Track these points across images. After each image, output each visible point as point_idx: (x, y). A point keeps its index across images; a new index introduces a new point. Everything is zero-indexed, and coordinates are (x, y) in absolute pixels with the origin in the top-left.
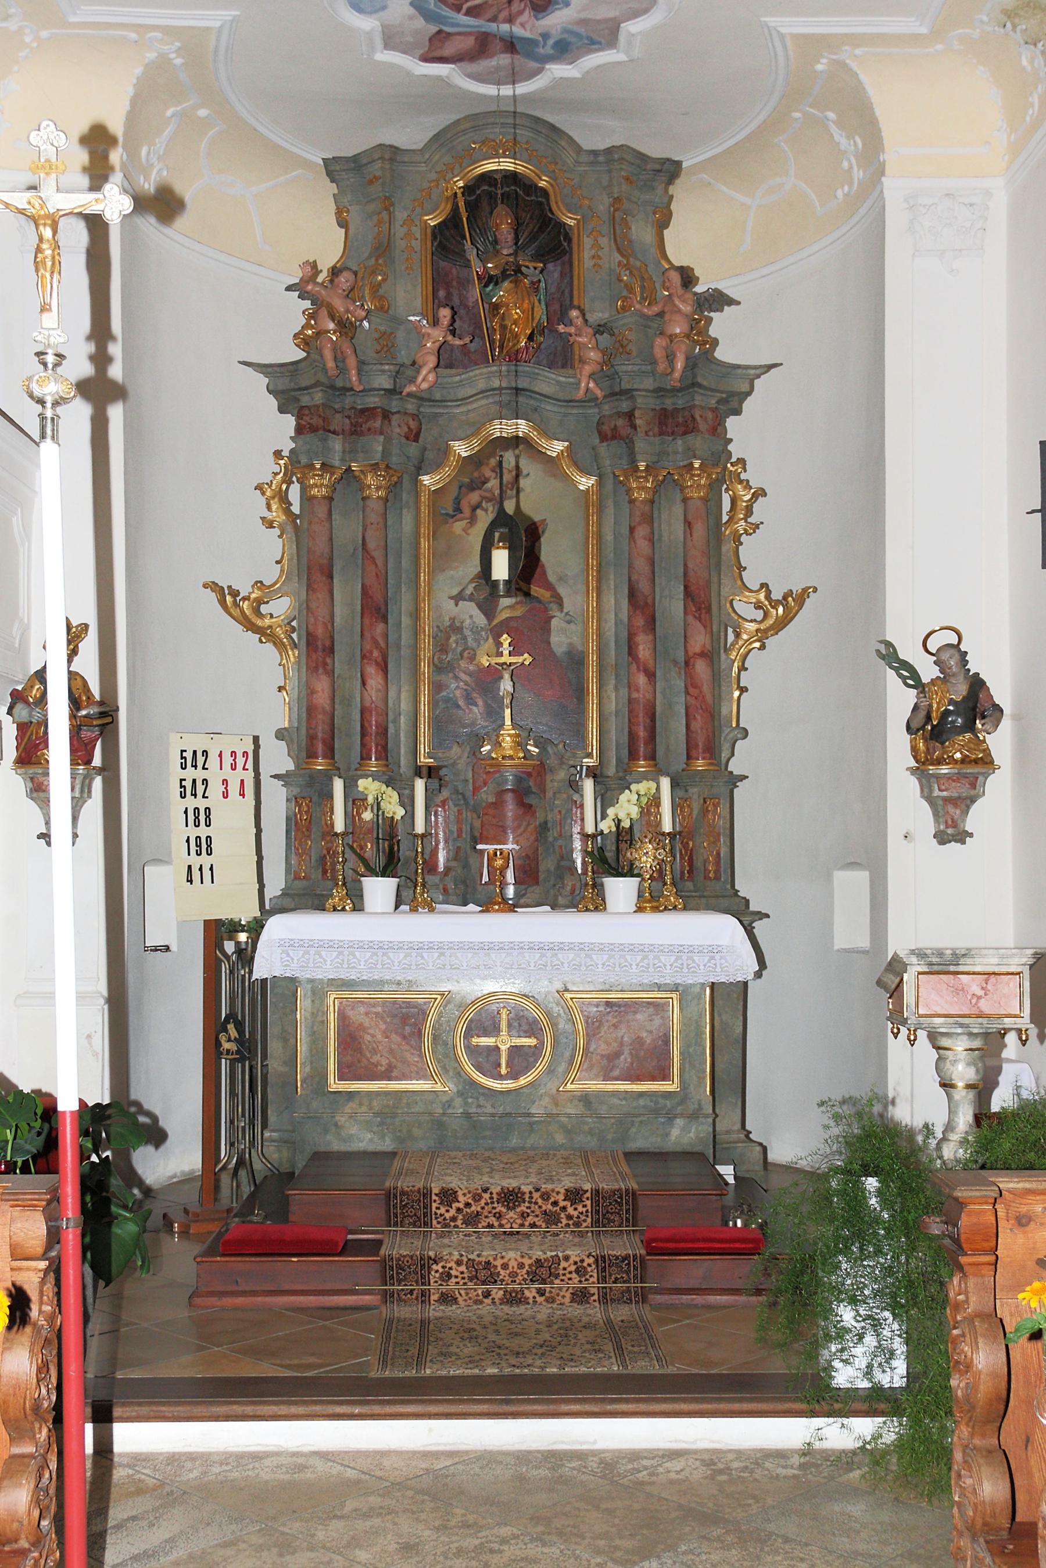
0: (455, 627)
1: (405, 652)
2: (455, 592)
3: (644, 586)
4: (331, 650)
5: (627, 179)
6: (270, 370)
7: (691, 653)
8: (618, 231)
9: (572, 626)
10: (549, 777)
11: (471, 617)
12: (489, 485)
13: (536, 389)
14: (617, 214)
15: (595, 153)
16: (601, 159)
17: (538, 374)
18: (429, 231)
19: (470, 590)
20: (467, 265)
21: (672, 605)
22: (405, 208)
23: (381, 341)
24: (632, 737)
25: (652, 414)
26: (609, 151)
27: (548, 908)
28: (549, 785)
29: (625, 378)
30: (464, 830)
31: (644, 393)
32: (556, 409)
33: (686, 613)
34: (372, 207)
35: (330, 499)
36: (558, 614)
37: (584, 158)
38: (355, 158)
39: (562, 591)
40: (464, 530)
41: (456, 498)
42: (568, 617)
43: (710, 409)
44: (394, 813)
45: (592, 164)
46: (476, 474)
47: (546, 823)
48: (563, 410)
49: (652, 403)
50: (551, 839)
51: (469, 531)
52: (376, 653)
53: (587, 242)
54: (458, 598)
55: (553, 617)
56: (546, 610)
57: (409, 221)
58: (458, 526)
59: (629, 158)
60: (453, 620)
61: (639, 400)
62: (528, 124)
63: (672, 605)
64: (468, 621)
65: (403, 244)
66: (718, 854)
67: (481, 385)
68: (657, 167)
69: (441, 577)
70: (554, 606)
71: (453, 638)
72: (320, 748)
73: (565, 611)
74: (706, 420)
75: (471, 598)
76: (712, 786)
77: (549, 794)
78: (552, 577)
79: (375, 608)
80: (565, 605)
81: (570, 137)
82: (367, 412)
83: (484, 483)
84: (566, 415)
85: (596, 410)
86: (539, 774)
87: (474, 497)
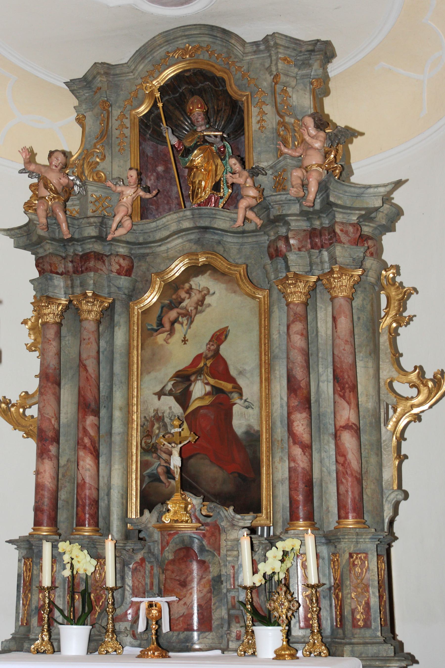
0: (158, 418)
1: (117, 439)
2: (158, 389)
3: (299, 373)
4: (56, 440)
5: (285, 59)
6: (13, 232)
7: (338, 427)
8: (279, 100)
9: (250, 410)
10: (223, 537)
11: (170, 408)
12: (184, 304)
13: (216, 226)
14: (278, 86)
15: (256, 44)
16: (262, 47)
17: (215, 214)
18: (137, 121)
19: (169, 387)
20: (163, 140)
21: (324, 385)
22: (120, 107)
23: (97, 203)
24: (293, 502)
25: (303, 234)
26: (266, 40)
27: (218, 652)
28: (223, 543)
29: (277, 207)
30: (154, 583)
31: (295, 218)
32: (235, 240)
33: (334, 393)
34: (96, 110)
35: (60, 325)
36: (238, 401)
37: (249, 49)
38: (85, 78)
39: (241, 382)
40: (165, 340)
41: (159, 316)
42: (246, 404)
43: (351, 224)
44: (85, 570)
45: (255, 52)
46: (174, 297)
47: (219, 576)
48: (240, 240)
49: (304, 225)
50: (224, 591)
51: (169, 341)
52: (86, 440)
53: (254, 111)
54: (160, 394)
55: (235, 404)
56: (229, 399)
57: (123, 116)
58: (161, 338)
59: (283, 42)
60: (156, 411)
61: (293, 224)
62: (207, 32)
63: (324, 385)
64: (168, 411)
65: (118, 132)
66: (368, 604)
67: (174, 227)
68: (310, 48)
69: (147, 378)
70: (235, 395)
71: (156, 426)
72: (45, 520)
73: (244, 398)
74: (346, 233)
75: (170, 393)
76: (357, 543)
77: (223, 551)
78: (233, 372)
79: (88, 406)
80: (244, 394)
81: (237, 36)
82: (86, 257)
83: (180, 303)
84: (242, 244)
85: (266, 238)
86: (213, 534)
87: (173, 314)
